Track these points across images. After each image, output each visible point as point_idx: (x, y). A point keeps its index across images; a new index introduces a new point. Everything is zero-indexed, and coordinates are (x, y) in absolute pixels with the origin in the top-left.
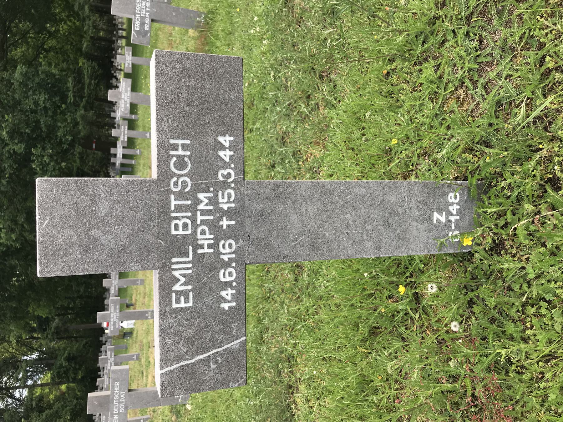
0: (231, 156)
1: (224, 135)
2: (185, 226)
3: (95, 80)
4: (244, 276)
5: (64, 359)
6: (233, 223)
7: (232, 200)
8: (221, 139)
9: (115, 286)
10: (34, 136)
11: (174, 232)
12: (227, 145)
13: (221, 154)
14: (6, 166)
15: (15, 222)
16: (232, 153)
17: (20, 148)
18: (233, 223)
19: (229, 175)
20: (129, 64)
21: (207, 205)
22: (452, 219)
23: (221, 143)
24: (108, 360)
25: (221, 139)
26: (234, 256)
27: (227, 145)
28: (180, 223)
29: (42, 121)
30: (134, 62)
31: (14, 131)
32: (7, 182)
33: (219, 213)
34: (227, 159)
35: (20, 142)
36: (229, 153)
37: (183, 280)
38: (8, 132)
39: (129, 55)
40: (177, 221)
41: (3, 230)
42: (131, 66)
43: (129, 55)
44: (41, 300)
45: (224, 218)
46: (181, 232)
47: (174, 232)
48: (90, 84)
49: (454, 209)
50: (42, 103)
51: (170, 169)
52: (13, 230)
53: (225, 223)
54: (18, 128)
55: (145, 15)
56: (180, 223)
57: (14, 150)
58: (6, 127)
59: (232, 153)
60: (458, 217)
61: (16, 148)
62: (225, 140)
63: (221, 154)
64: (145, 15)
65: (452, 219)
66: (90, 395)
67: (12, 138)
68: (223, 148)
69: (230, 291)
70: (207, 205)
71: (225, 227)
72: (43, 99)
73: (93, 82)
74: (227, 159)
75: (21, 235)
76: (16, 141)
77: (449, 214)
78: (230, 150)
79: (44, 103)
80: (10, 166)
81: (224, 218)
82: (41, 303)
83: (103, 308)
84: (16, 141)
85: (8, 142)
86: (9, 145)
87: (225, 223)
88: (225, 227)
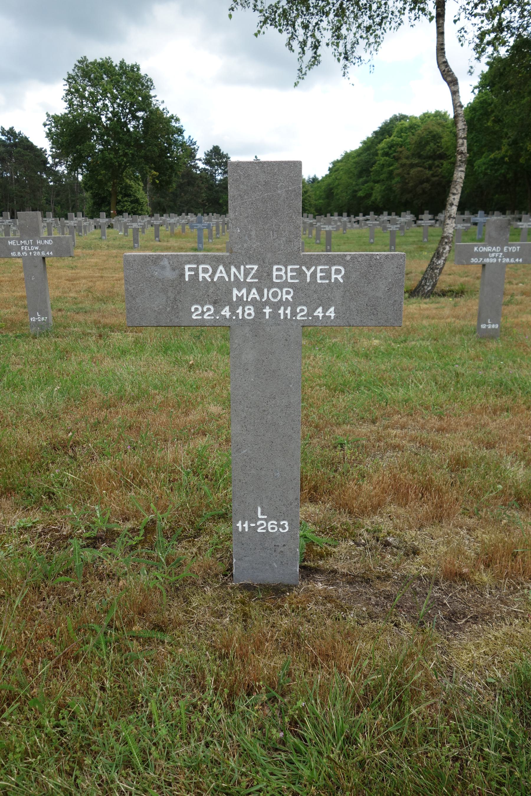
1: (230, 311)
2: (279, 277)
4: (144, 325)
6: (267, 317)
8: (332, 309)
11: (275, 267)
13: (320, 309)
18: (267, 317)
19: (284, 528)
21: (237, 296)
23: (329, 308)
25: (332, 309)
26: (240, 318)
28: (282, 273)
33: (276, 307)
34: (315, 314)
36: (321, 315)
37: (240, 295)
40: (284, 271)
45: (271, 310)
46: (275, 273)
47: (275, 267)
51: (210, 264)
53: (267, 310)
55: (24, 251)
56: (282, 273)
63: (320, 309)
64: (24, 251)
68: (325, 310)
69: (228, 314)
70: (237, 296)
71: (264, 311)
81: (271, 310)
87: (267, 310)
88: (264, 311)
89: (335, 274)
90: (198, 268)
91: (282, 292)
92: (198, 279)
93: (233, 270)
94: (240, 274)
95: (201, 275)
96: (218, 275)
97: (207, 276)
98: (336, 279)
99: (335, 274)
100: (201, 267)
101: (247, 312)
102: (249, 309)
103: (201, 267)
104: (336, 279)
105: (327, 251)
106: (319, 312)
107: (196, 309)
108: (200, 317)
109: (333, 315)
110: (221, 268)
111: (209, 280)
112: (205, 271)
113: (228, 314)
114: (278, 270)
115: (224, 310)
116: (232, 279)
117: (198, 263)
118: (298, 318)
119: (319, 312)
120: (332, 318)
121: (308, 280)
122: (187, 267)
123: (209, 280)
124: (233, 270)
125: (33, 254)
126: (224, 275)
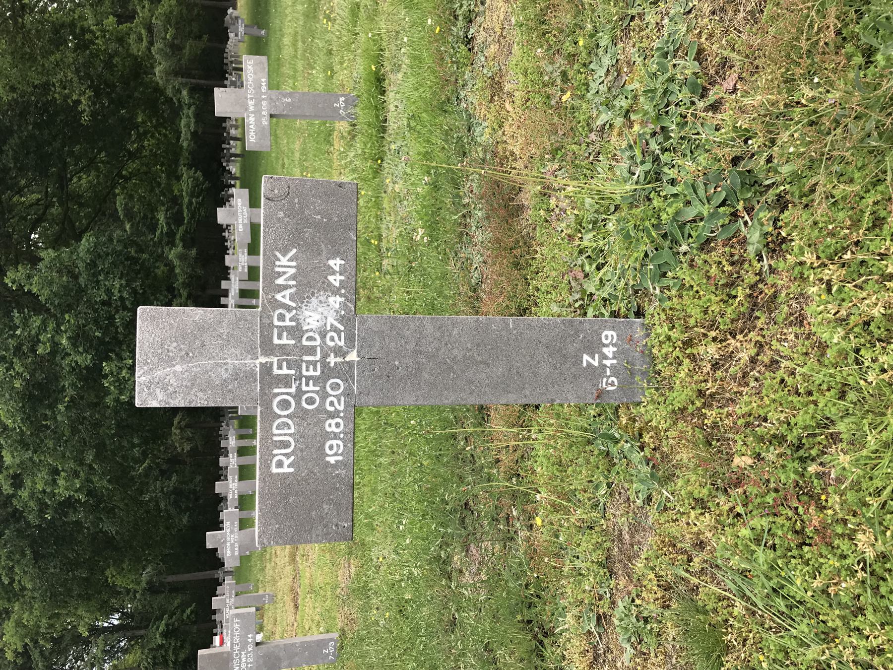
0: (341, 281)
1: (334, 258)
3: (198, 197)
5: (160, 634)
7: (340, 452)
8: (331, 263)
9: (232, 545)
10: (107, 340)
12: (337, 269)
13: (331, 278)
14: (67, 384)
15: (81, 463)
16: (343, 278)
17: (84, 359)
20: (243, 267)
22: (608, 363)
24: (227, 604)
25: (331, 263)
27: (337, 269)
29: (117, 316)
30: (251, 265)
31: (78, 335)
32: (67, 407)
34: (337, 284)
35: (86, 351)
36: (339, 278)
38: (69, 338)
39: (243, 254)
41: (62, 473)
42: (246, 270)
43: (243, 254)
44: (123, 561)
47: (275, 470)
48: (190, 203)
49: (609, 351)
50: (116, 291)
52: (76, 474)
54: (84, 332)
57: (76, 362)
58: (66, 332)
59: (343, 278)
60: (615, 361)
61: (79, 359)
62: (336, 263)
63: (331, 278)
65: (608, 363)
66: (201, 652)
67: (75, 345)
68: (334, 273)
71: (332, 365)
72: (118, 286)
73: (194, 200)
74: (337, 284)
75: (88, 480)
76: (80, 349)
77: (604, 357)
78: (341, 275)
79: (119, 291)
80: (73, 385)
82: (125, 566)
83: (217, 525)
84: (80, 349)
85: (68, 351)
86: (70, 355)
88: (332, 365)
89: (284, 321)
90: (277, 327)
91: (308, 392)
92: (292, 327)
93: (280, 281)
94: (285, 273)
95: (287, 323)
96: (287, 301)
97: (287, 462)
98: (289, 466)
99: (284, 321)
100: (276, 323)
101: (334, 429)
102: (330, 425)
103: (276, 323)
104: (289, 466)
105: (254, 453)
106: (335, 280)
107: (332, 404)
108: (343, 334)
109: (339, 261)
110: (278, 297)
111: (293, 458)
112: (282, 318)
113: (339, 278)
114: (280, 464)
115: (334, 267)
116: (294, 283)
117: (271, 326)
118: (341, 408)
119: (335, 280)
120: (343, 262)
121: (295, 250)
122: (276, 341)
123: (293, 458)
124: (280, 281)
125: (251, 663)
126: (287, 292)
